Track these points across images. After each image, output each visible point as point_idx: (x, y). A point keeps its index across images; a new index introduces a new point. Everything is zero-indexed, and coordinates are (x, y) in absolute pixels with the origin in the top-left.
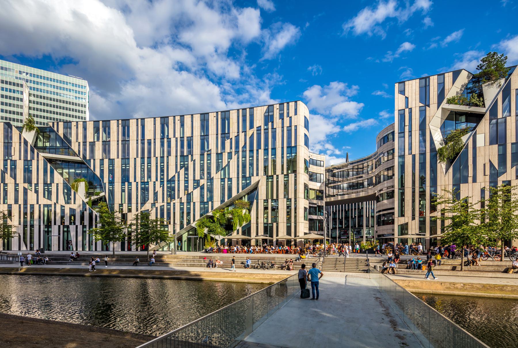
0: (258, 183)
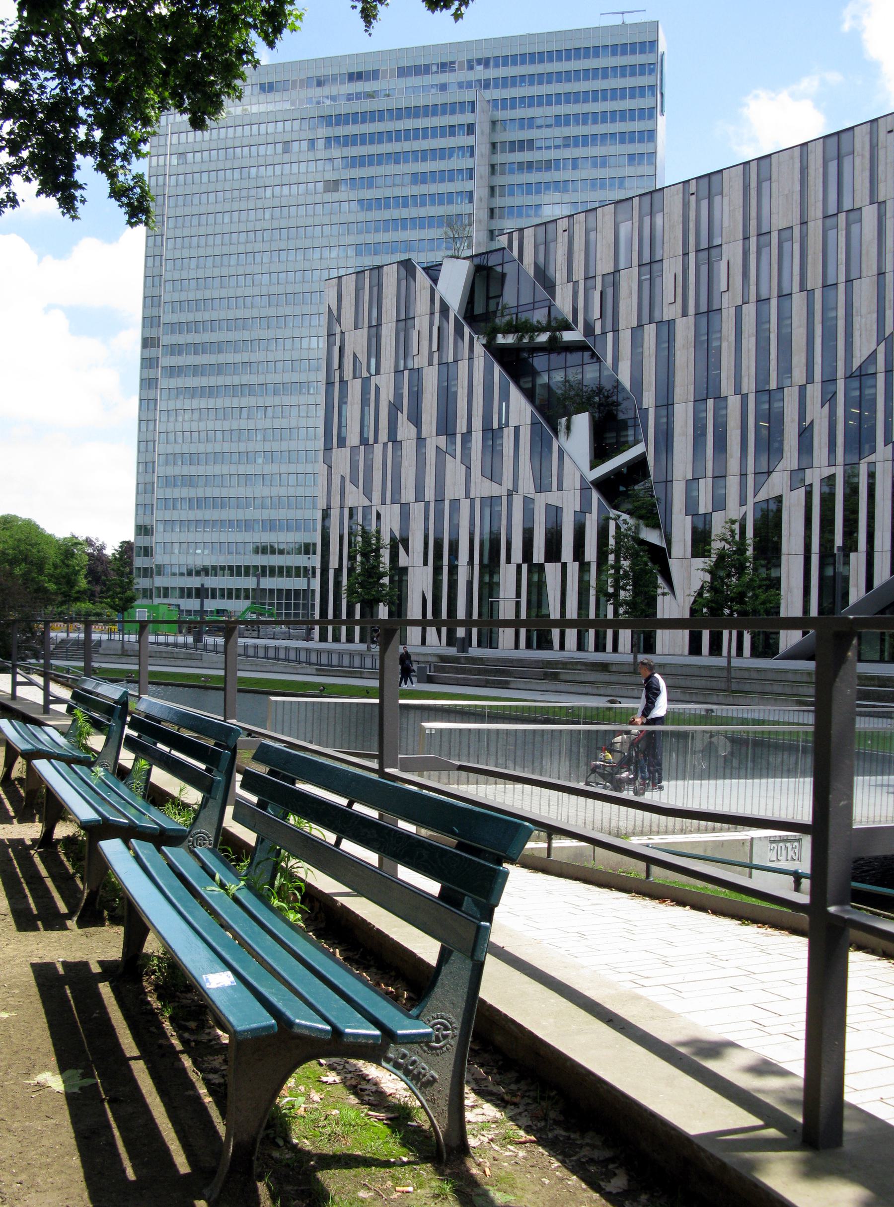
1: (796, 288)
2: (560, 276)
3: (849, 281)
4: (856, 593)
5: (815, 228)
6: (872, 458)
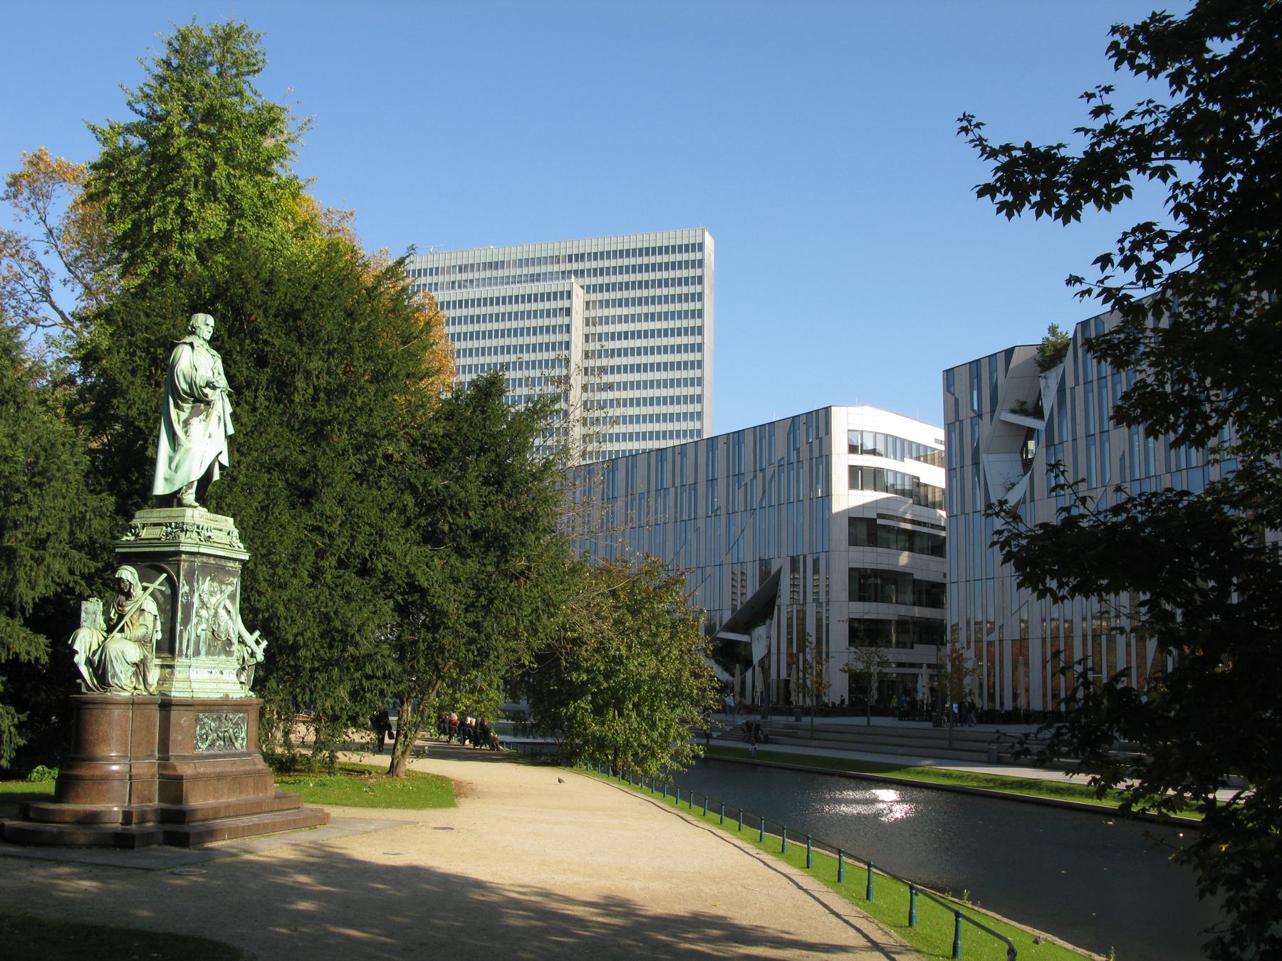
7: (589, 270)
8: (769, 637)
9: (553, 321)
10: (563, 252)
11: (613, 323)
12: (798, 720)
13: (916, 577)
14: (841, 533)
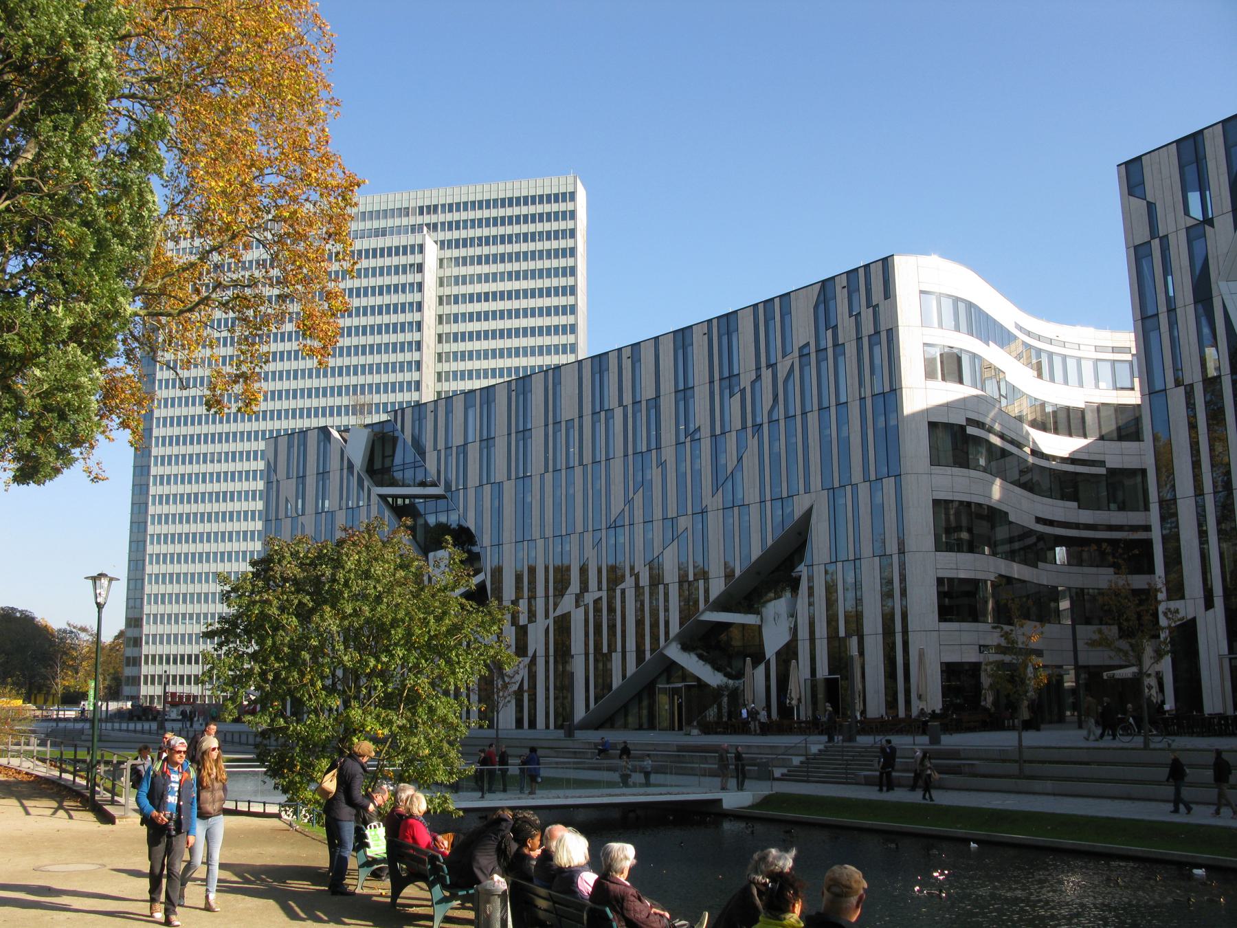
0: (808, 514)
1: (577, 463)
2: (429, 446)
3: (607, 460)
4: (617, 681)
5: (587, 420)
6: (622, 586)
7: (443, 224)
8: (793, 614)
9: (402, 279)
10: (413, 204)
11: (472, 282)
12: (935, 740)
13: (1075, 504)
14: (916, 447)
